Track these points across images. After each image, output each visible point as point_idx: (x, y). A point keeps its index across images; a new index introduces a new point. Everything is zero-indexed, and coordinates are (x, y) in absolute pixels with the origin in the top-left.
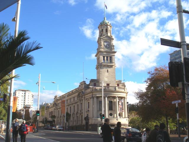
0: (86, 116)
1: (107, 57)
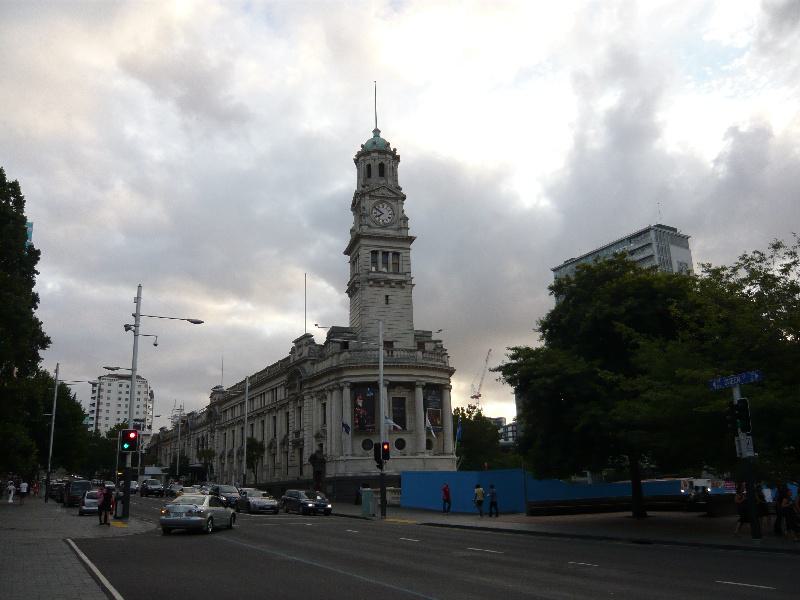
0: (314, 452)
1: (386, 254)
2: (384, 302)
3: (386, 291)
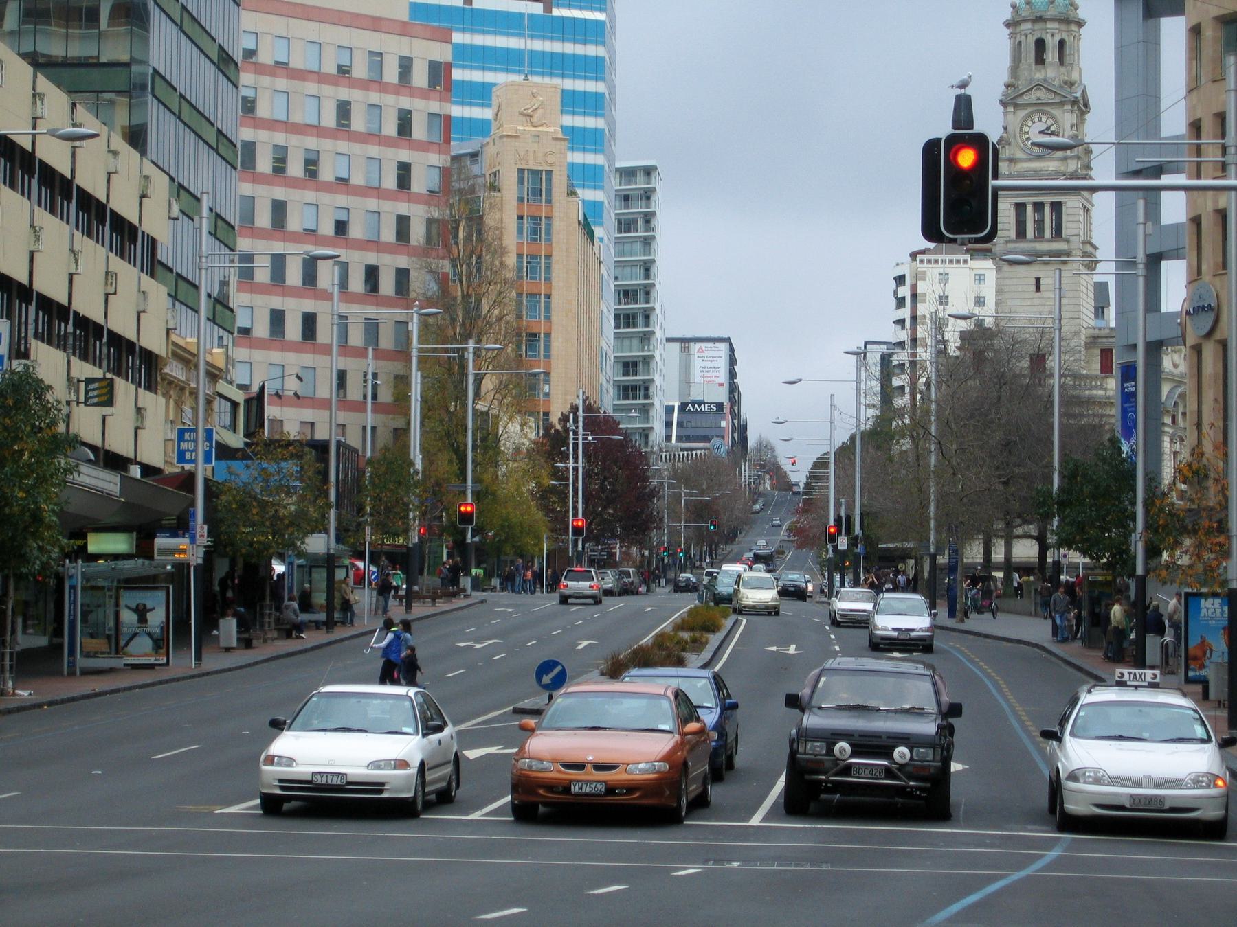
1: (1038, 207)
2: (1034, 288)
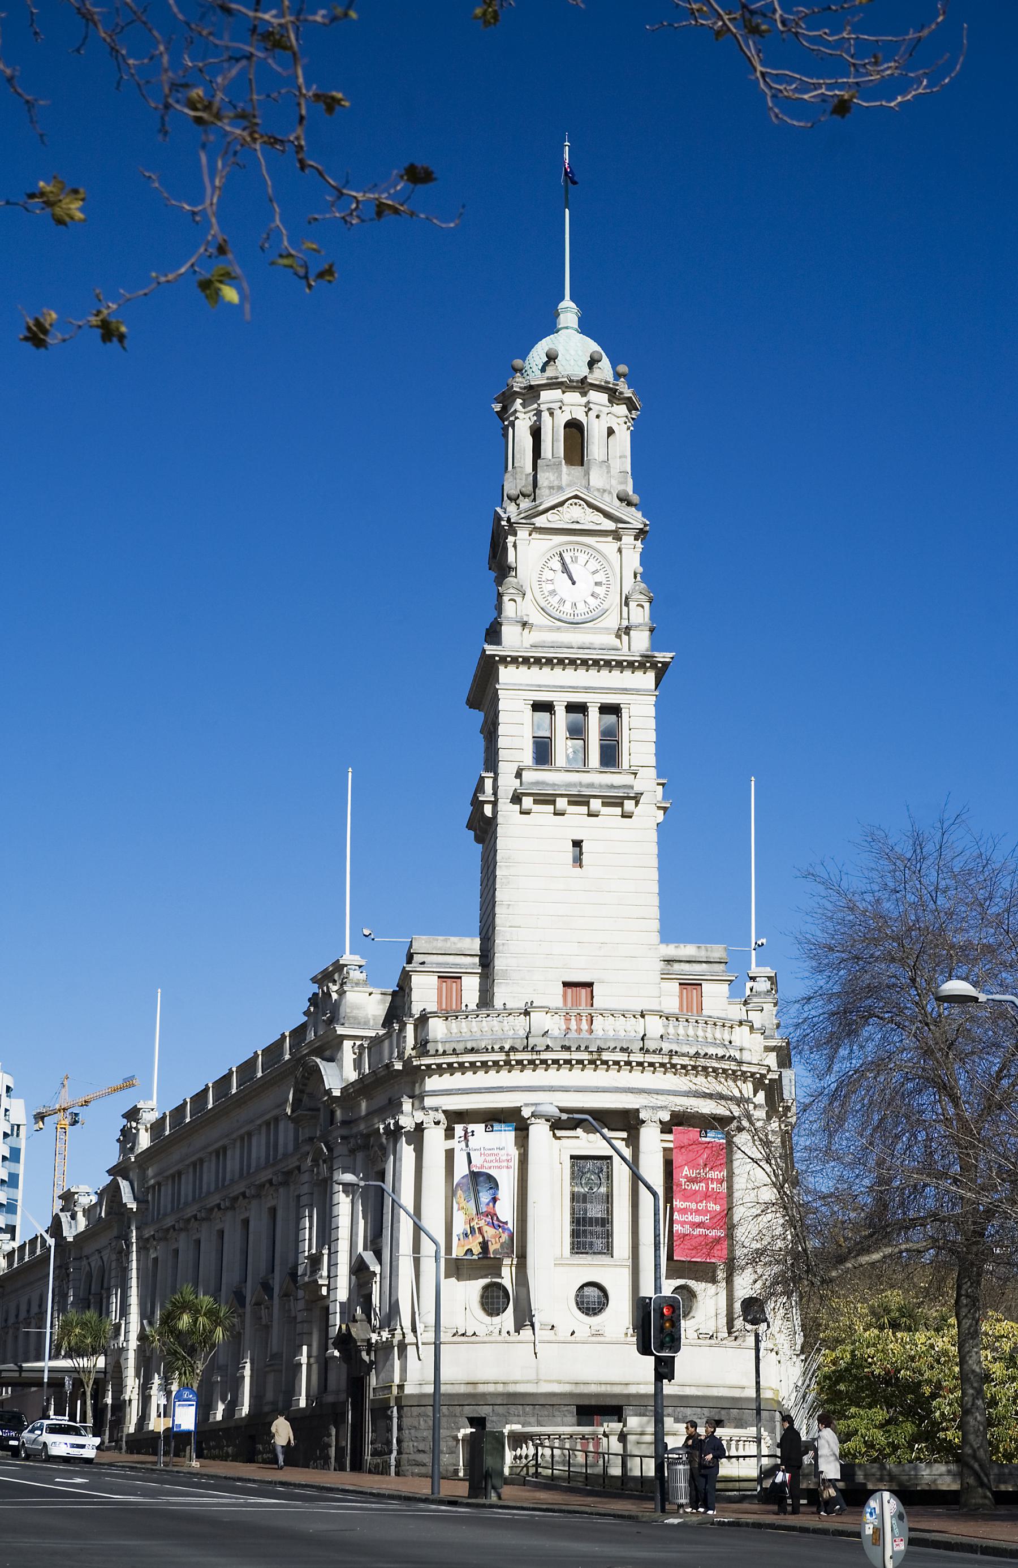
3: (576, 822)
